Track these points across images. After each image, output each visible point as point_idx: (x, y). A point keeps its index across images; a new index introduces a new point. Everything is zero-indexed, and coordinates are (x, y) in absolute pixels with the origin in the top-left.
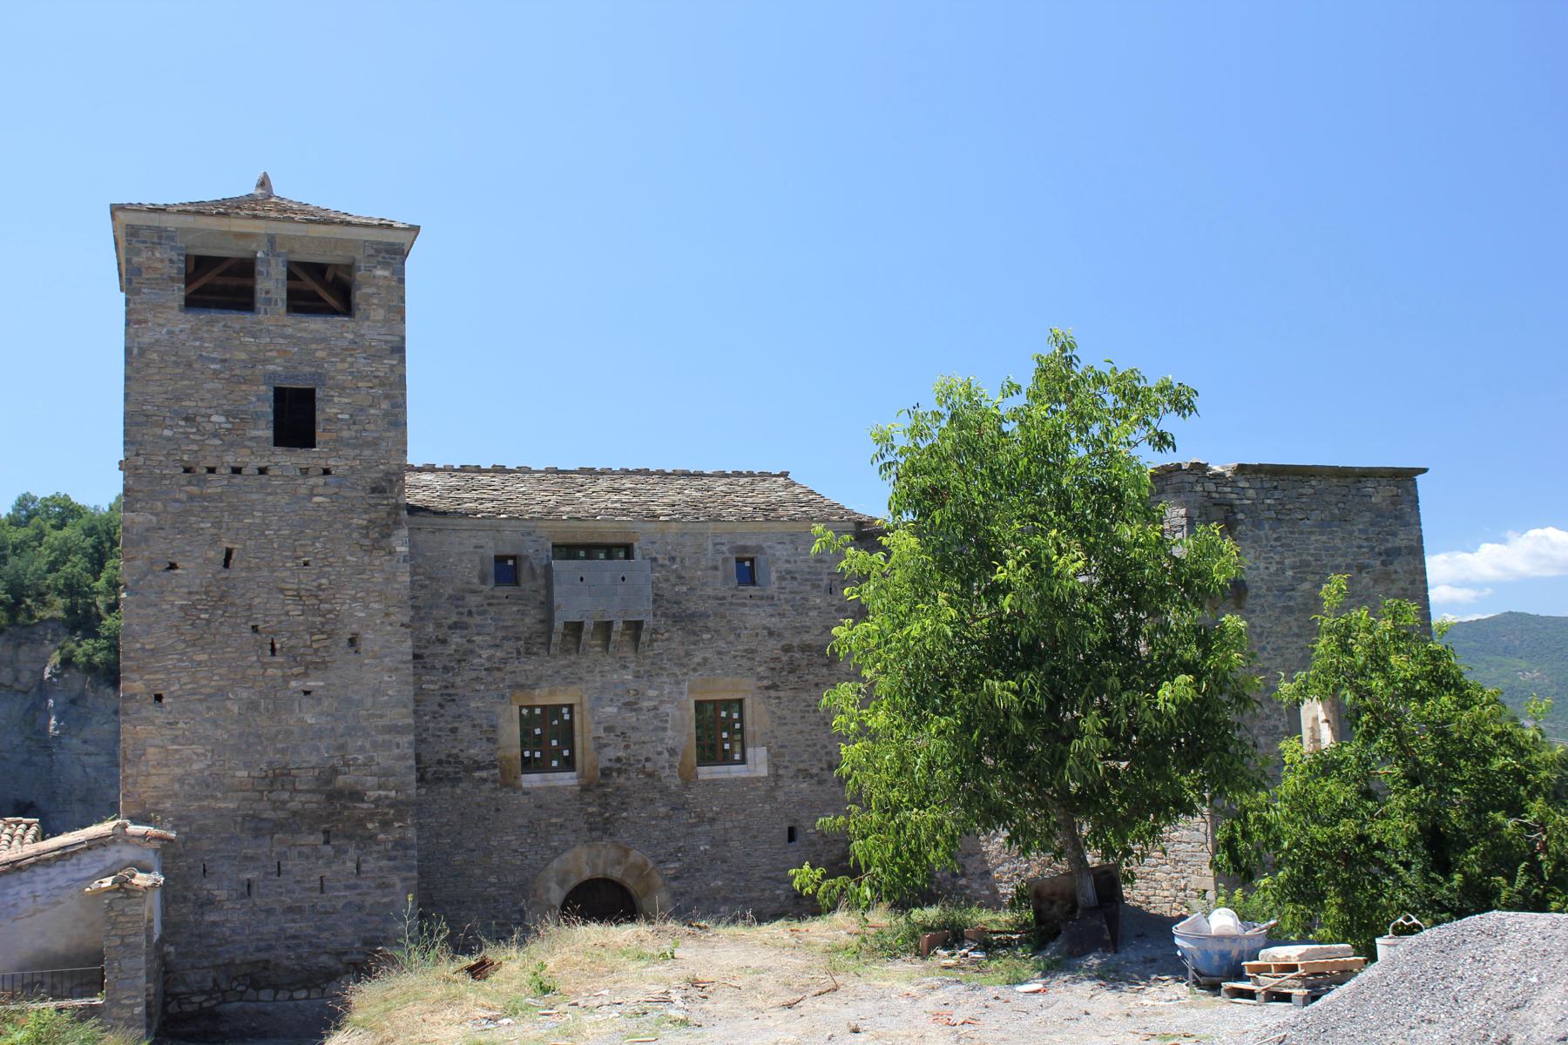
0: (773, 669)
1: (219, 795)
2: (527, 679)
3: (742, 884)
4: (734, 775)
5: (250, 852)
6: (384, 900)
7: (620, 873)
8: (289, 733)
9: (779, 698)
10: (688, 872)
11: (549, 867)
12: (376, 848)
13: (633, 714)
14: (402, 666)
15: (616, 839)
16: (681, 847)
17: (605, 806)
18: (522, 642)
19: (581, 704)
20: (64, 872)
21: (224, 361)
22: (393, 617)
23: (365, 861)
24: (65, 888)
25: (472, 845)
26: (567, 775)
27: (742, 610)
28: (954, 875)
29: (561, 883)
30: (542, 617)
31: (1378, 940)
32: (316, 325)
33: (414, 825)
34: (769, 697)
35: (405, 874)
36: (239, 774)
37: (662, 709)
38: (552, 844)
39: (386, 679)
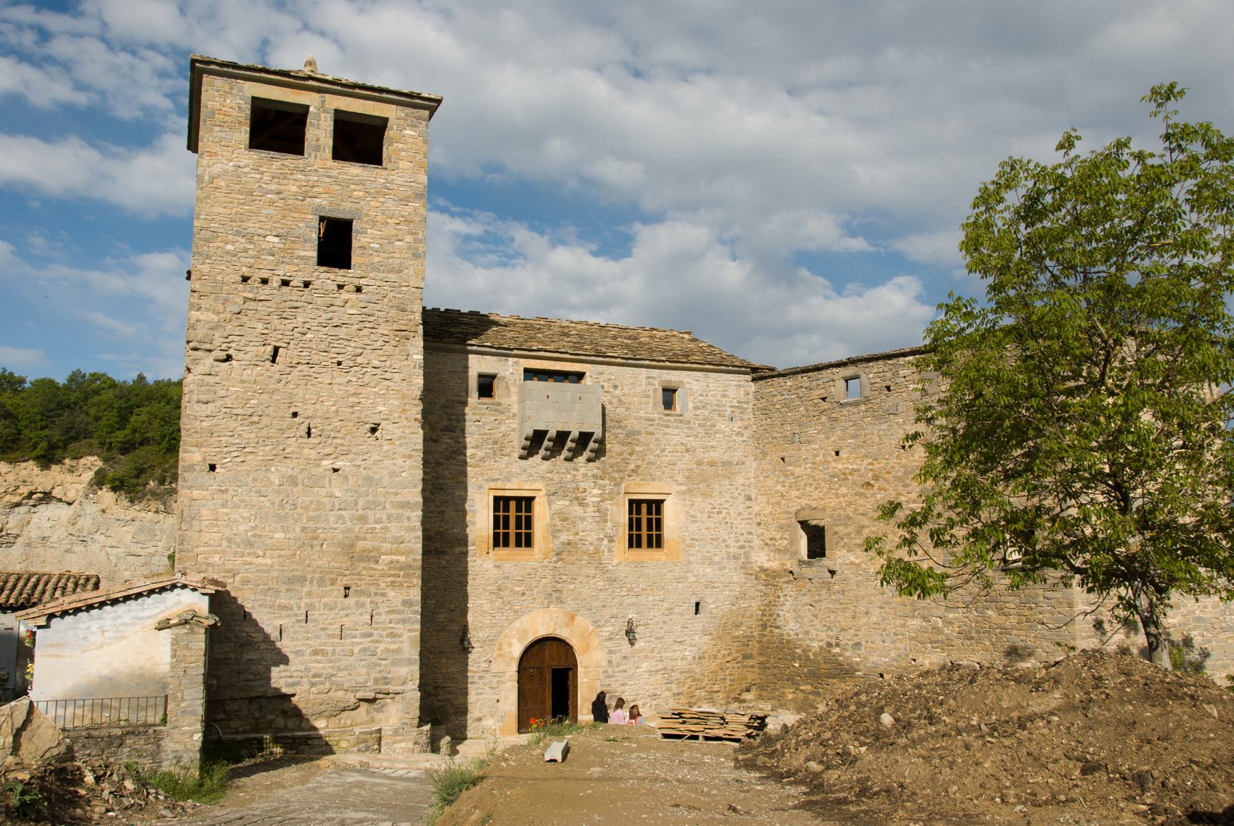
1: (260, 553)
3: (659, 646)
5: (283, 602)
22: (409, 413)
23: (378, 614)
24: (131, 624)
25: (452, 606)
28: (829, 645)
31: (273, 668)
32: (354, 170)
35: (408, 626)
36: (276, 535)
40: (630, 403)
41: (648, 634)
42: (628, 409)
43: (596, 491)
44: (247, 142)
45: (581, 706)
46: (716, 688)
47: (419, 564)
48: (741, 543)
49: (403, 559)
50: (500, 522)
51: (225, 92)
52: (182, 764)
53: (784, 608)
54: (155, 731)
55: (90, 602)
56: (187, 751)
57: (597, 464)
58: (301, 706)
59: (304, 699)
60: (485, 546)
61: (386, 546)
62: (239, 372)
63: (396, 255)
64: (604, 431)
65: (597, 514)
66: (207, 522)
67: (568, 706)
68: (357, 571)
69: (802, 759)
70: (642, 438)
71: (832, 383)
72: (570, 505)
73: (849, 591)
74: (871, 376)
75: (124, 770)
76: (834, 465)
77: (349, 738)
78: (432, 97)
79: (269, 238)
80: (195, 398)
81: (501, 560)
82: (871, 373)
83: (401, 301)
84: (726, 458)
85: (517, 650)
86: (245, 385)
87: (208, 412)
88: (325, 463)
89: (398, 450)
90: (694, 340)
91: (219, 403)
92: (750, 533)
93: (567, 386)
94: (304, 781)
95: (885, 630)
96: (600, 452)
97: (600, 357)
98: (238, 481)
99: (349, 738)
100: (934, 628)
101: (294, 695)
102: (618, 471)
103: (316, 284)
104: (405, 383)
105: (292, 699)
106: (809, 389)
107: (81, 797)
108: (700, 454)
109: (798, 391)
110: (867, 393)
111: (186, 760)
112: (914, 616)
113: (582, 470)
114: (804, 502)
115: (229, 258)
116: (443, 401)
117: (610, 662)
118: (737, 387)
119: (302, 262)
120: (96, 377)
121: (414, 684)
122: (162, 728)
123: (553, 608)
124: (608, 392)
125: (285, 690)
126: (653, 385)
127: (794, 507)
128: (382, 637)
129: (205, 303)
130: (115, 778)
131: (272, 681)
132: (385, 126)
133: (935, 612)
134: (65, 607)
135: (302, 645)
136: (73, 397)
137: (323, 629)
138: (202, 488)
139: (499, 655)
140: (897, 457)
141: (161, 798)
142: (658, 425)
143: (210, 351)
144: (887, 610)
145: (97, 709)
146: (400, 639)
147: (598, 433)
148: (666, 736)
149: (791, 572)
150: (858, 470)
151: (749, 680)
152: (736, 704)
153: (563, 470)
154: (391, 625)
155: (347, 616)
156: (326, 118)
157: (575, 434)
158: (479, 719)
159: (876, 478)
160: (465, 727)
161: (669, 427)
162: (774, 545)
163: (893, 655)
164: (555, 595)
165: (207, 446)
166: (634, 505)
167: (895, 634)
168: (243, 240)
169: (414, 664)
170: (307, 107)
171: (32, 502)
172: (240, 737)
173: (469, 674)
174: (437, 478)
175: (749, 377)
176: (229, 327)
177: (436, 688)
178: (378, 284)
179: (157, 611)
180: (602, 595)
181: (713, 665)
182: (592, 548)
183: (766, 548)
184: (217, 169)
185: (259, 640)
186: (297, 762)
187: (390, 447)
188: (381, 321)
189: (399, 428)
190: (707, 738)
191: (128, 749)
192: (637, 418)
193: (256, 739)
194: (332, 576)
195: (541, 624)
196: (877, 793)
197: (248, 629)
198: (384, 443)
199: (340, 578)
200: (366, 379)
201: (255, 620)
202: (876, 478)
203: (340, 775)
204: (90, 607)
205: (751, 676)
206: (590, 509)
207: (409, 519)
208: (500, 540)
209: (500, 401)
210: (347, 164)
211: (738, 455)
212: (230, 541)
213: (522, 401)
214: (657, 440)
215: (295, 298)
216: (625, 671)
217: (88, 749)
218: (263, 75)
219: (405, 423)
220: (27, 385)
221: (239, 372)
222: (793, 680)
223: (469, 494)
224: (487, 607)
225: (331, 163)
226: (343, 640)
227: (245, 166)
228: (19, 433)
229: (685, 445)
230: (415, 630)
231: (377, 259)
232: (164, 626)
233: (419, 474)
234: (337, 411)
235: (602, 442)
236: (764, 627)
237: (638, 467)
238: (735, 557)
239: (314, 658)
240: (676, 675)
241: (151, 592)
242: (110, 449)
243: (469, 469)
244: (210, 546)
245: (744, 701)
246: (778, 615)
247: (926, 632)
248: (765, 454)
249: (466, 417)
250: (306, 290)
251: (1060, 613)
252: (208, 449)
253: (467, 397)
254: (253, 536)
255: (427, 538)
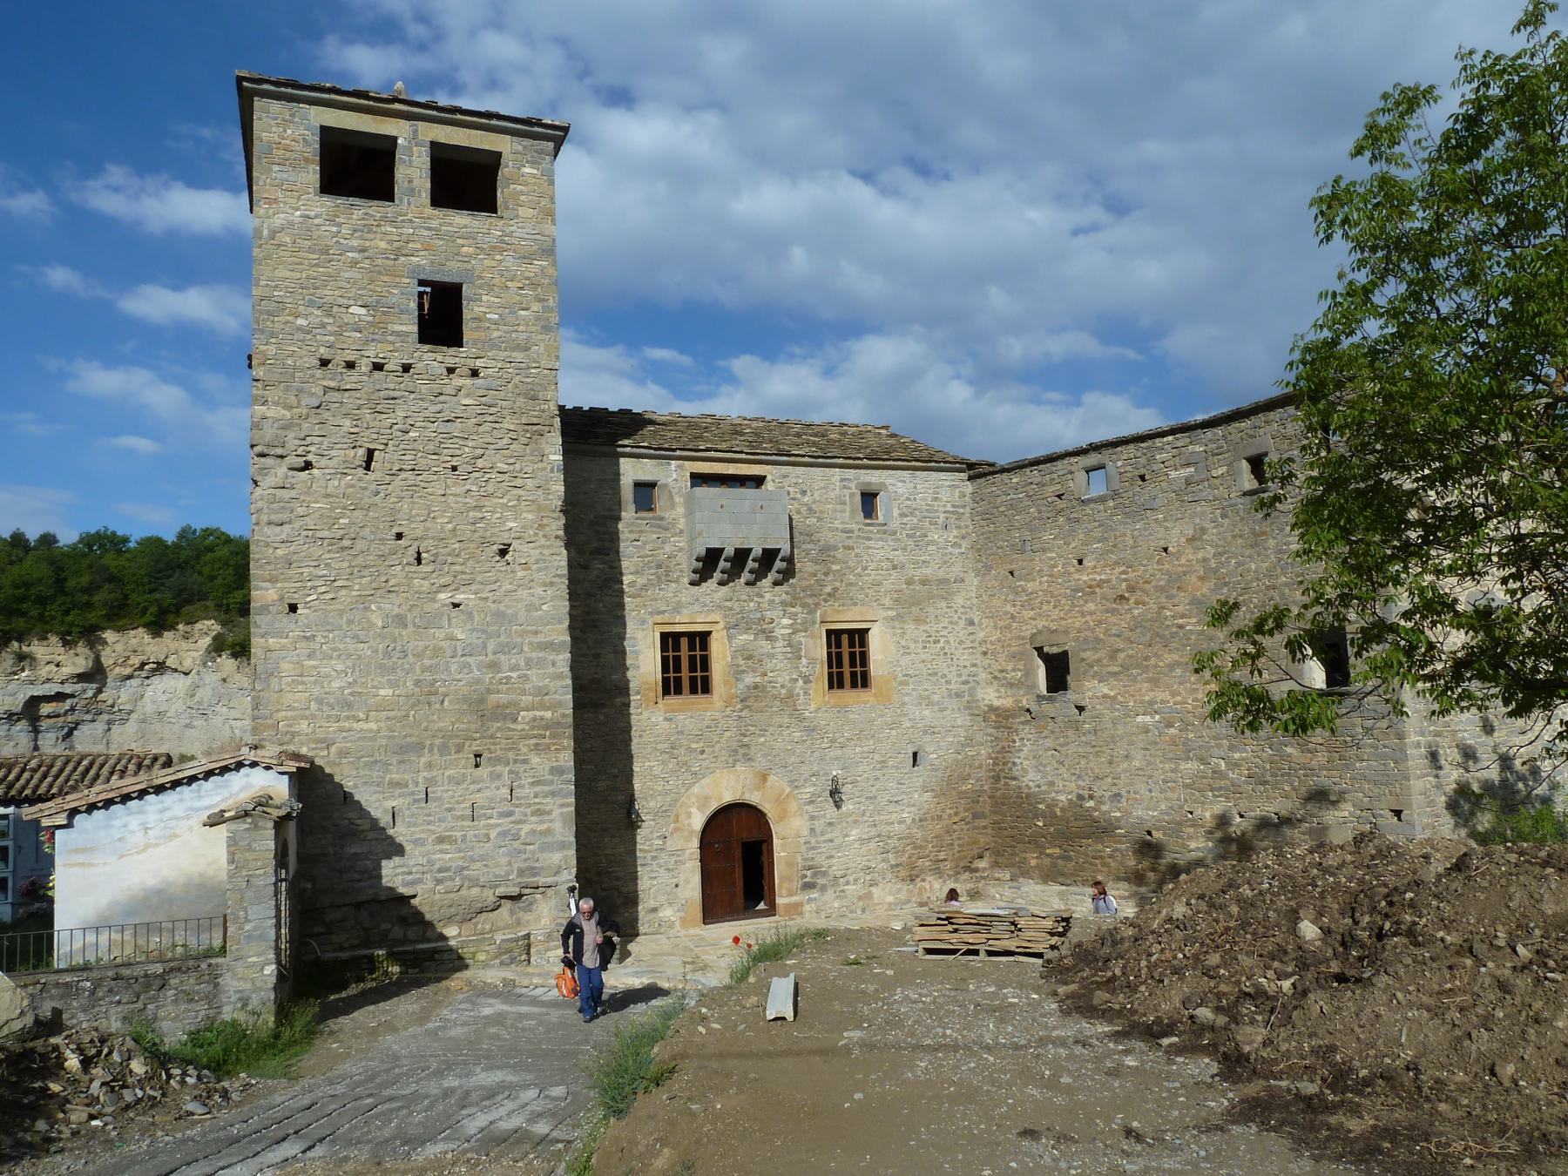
1: (361, 715)
5: (396, 777)
8: (437, 651)
20: (181, 800)
21: (362, 251)
22: (547, 529)
24: (183, 818)
28: (1080, 797)
31: (384, 863)
32: (461, 220)
35: (560, 801)
36: (382, 692)
40: (822, 512)
41: (857, 794)
42: (820, 519)
43: (786, 621)
44: (318, 185)
45: (780, 885)
46: (942, 856)
47: (570, 720)
48: (964, 678)
49: (548, 714)
50: (669, 664)
51: (283, 120)
52: (249, 1008)
53: (1022, 754)
54: (210, 965)
55: (125, 791)
56: (256, 989)
57: (784, 588)
58: (423, 909)
59: (428, 898)
60: (652, 694)
61: (526, 700)
62: (322, 483)
63: (521, 328)
64: (792, 547)
65: (788, 649)
66: (290, 679)
67: (762, 887)
68: (490, 733)
69: (1177, 1002)
70: (839, 554)
71: (1069, 476)
72: (755, 640)
73: (1102, 730)
74: (1120, 464)
75: (130, 1044)
76: (1076, 576)
77: (488, 948)
78: (557, 123)
79: (354, 309)
80: (265, 518)
81: (673, 711)
82: (1118, 462)
83: (529, 387)
84: (941, 574)
85: (698, 821)
86: (332, 500)
87: (284, 537)
88: (442, 596)
89: (535, 576)
90: (893, 436)
91: (297, 525)
92: (975, 665)
93: (748, 493)
94: (423, 1017)
95: (1151, 777)
96: (788, 573)
97: (784, 457)
98: (329, 624)
99: (488, 948)
100: (1214, 772)
101: (414, 896)
102: (811, 596)
103: (419, 367)
104: (540, 492)
105: (412, 901)
106: (1041, 485)
107: (55, 1095)
108: (910, 571)
109: (1027, 488)
110: (1116, 485)
111: (255, 1002)
112: (1188, 759)
113: (768, 596)
114: (1041, 624)
115: (302, 336)
116: (592, 517)
117: (813, 830)
118: (950, 489)
119: (399, 339)
120: (208, 532)
121: (570, 874)
122: (220, 960)
123: (739, 767)
124: (794, 499)
125: (402, 890)
126: (850, 488)
127: (1028, 630)
128: (526, 815)
129: (272, 395)
130: (116, 1057)
131: (384, 881)
132: (499, 164)
133: (1215, 751)
134: (92, 799)
135: (423, 831)
136: (184, 555)
137: (450, 810)
138: (281, 634)
139: (676, 829)
140: (1158, 562)
141: (190, 1081)
142: (858, 537)
143: (282, 457)
144: (1153, 752)
145: (142, 931)
146: (549, 817)
147: (785, 549)
148: (929, 951)
149: (1028, 710)
150: (1108, 581)
151: (982, 845)
152: (967, 874)
153: (744, 597)
154: (536, 800)
155: (479, 791)
156: (420, 152)
157: (757, 552)
158: (655, 910)
159: (1132, 589)
160: (636, 920)
161: (870, 539)
162: (1005, 678)
163: (1163, 807)
164: (742, 751)
165: (285, 580)
166: (834, 636)
167: (1165, 781)
168: (319, 313)
169: (569, 848)
170: (395, 139)
171: (144, 674)
172: (344, 955)
173: (638, 854)
174: (588, 613)
175: (964, 476)
176: (306, 426)
177: (599, 874)
178: (499, 365)
179: (219, 798)
180: (799, 749)
181: (938, 828)
182: (783, 691)
183: (995, 683)
184: (279, 220)
185: (365, 828)
186: (418, 983)
187: (526, 573)
188: (506, 412)
189: (535, 548)
190: (990, 953)
191: (173, 992)
192: (831, 530)
193: (365, 956)
194: (457, 741)
195: (726, 788)
196: (1367, 1082)
197: (350, 815)
198: (518, 568)
199: (468, 743)
200: (490, 488)
201: (358, 802)
202: (1132, 589)
203: (473, 1003)
204: (126, 798)
205: (983, 840)
206: (780, 643)
207: (554, 664)
208: (670, 686)
209: (662, 514)
210: (451, 212)
211: (956, 570)
212: (320, 702)
213: (690, 513)
214: (857, 555)
215: (392, 386)
216: (831, 841)
217: (117, 994)
218: (333, 96)
219: (543, 541)
220: (132, 545)
221: (322, 483)
222: (1036, 842)
223: (629, 630)
224: (657, 770)
225: (429, 211)
226: (476, 823)
227: (316, 216)
228: (126, 597)
229: (892, 560)
230: (568, 805)
231: (496, 334)
232: (215, 821)
233: (565, 605)
234: (454, 530)
235: (790, 560)
236: (997, 779)
237: (835, 590)
238: (958, 695)
239: (438, 847)
240: (893, 843)
241: (209, 774)
242: (227, 611)
243: (627, 600)
244: (294, 709)
245: (977, 870)
246: (1014, 763)
247: (1205, 778)
248: (988, 568)
249: (621, 536)
250: (406, 375)
251: (1385, 747)
252: (286, 585)
253: (620, 510)
254: (351, 694)
255: (579, 688)
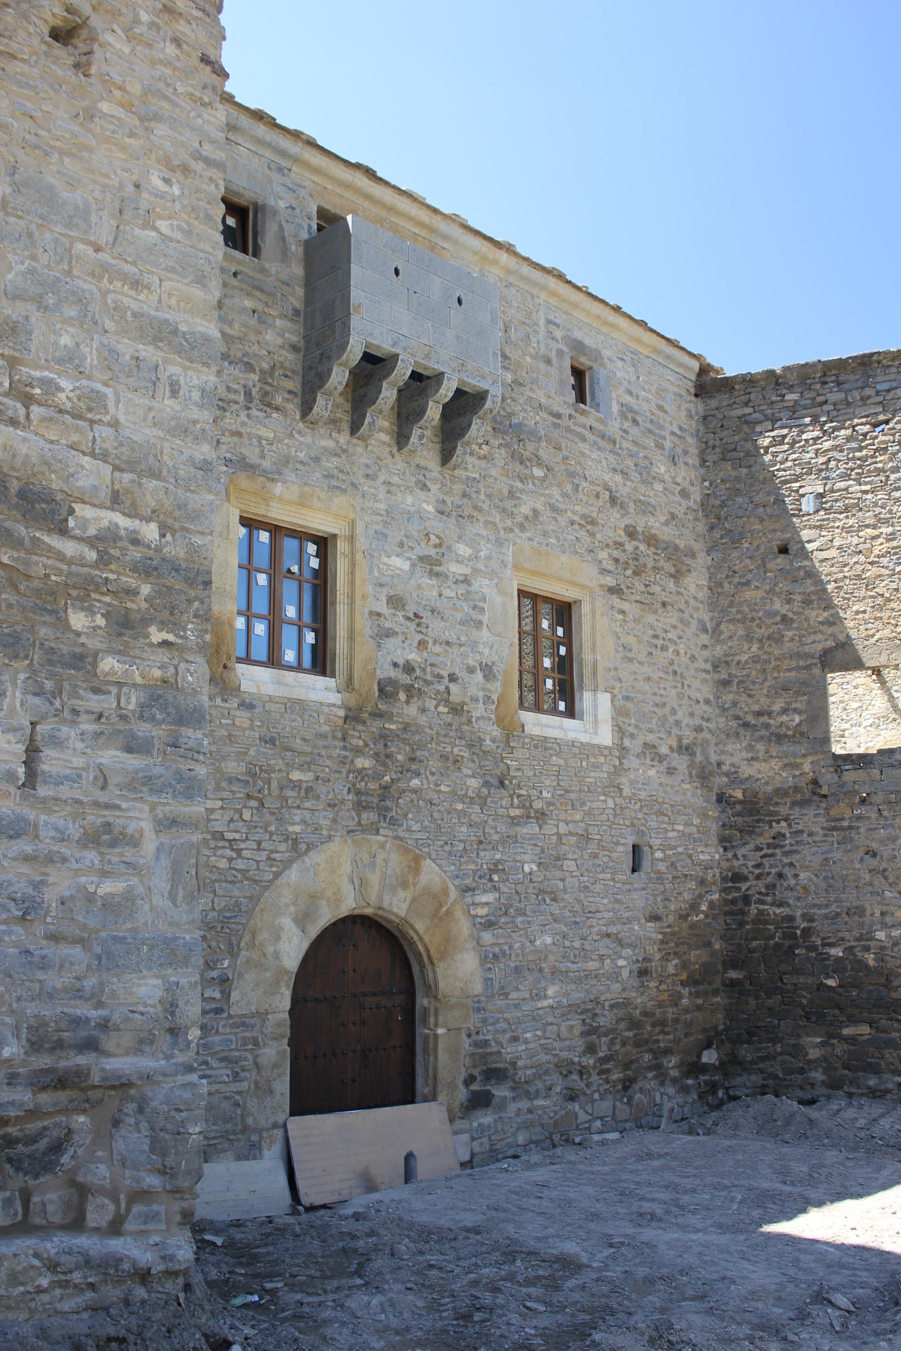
0: (617, 561)
2: (263, 457)
4: (571, 736)
6: (108, 887)
7: (405, 906)
9: (622, 612)
10: (506, 913)
11: (283, 879)
12: (94, 702)
13: (434, 582)
14: (199, 166)
15: (402, 834)
16: (498, 862)
17: (384, 758)
18: (255, 377)
19: (352, 539)
23: (55, 741)
26: (320, 681)
27: (582, 446)
29: (302, 921)
30: (294, 339)
33: (201, 648)
34: (612, 607)
37: (475, 586)
38: (291, 829)
39: (157, 182)
162: (767, 726)
